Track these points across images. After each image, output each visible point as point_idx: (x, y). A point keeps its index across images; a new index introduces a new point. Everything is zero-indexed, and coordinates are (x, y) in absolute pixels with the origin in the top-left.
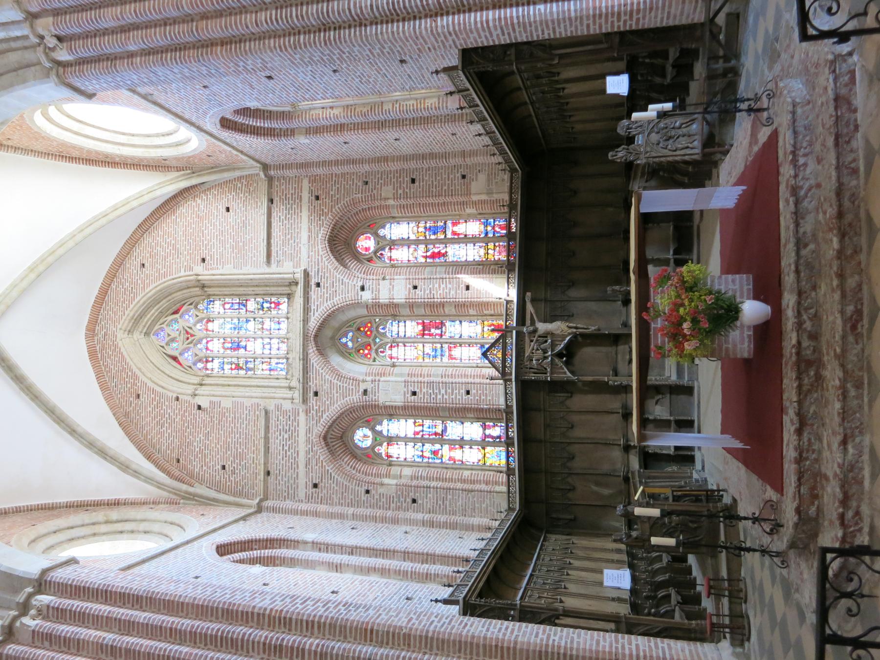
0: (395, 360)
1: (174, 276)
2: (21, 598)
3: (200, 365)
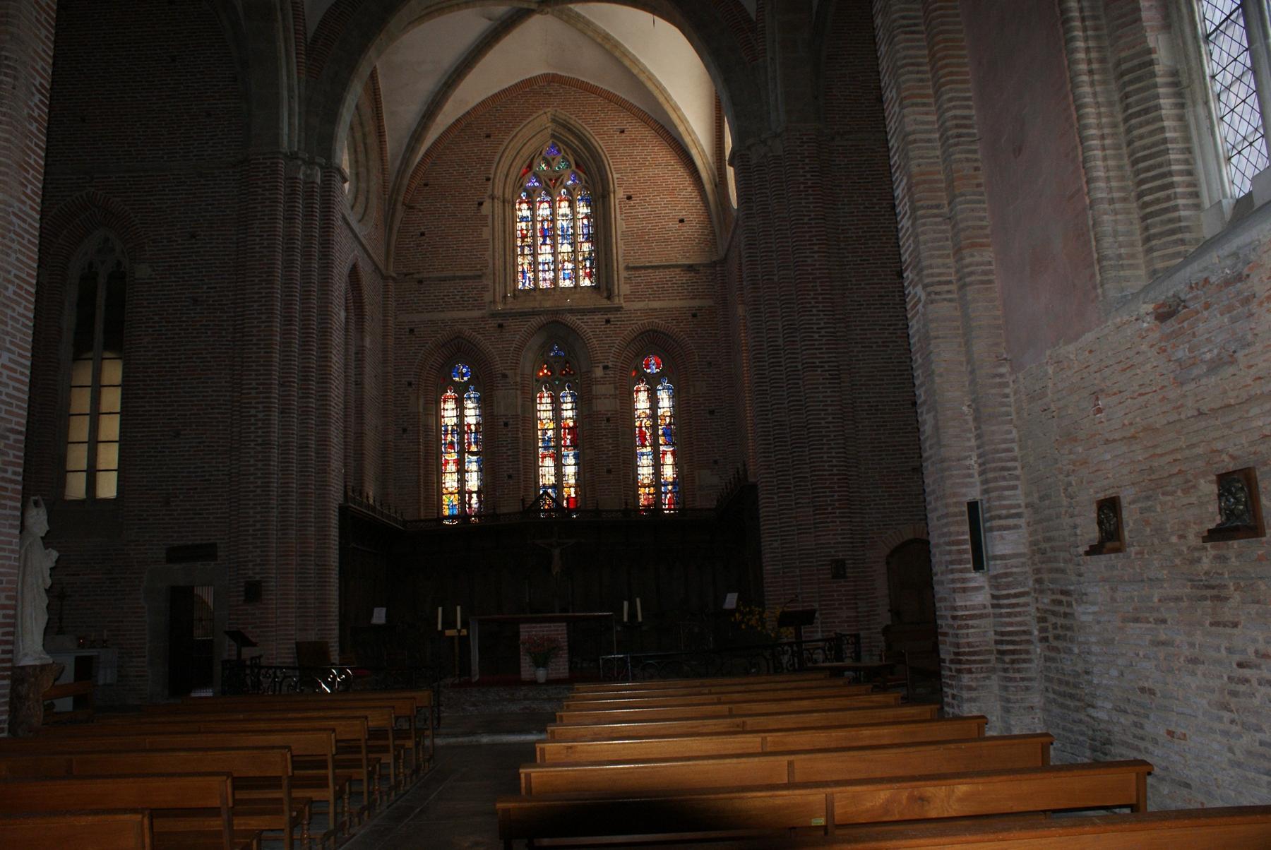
1: (612, 167)
2: (318, 160)
3: (523, 195)
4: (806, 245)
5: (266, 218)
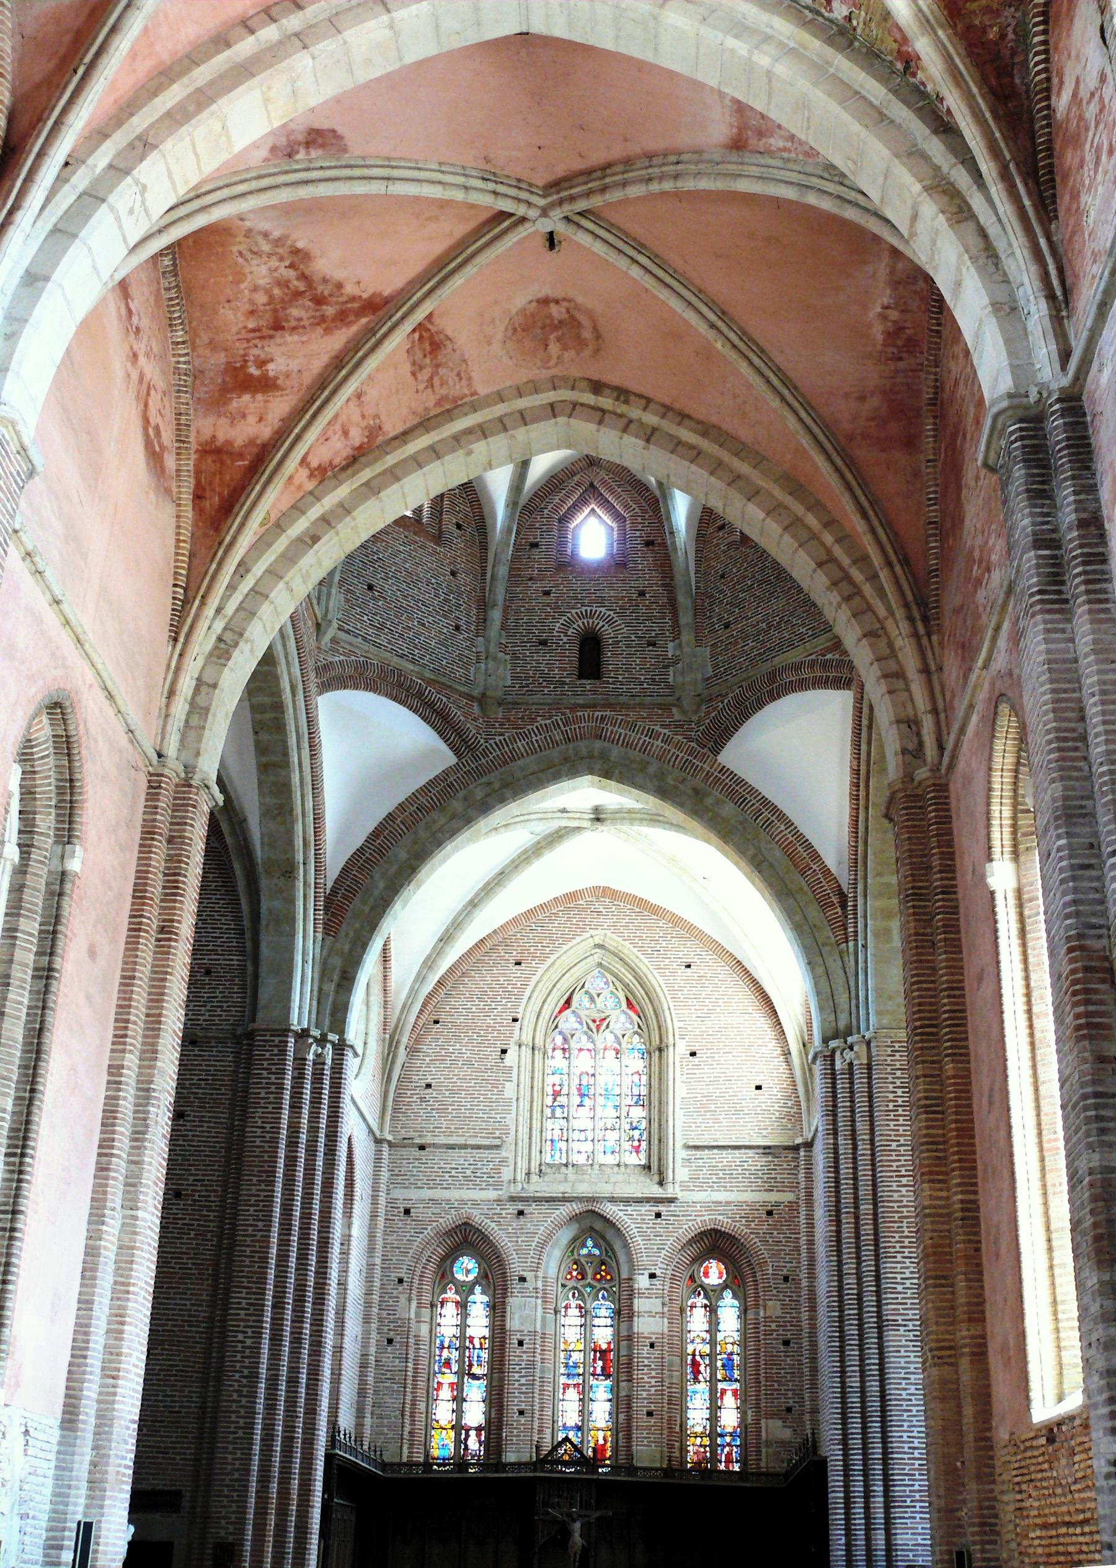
3: (559, 1040)
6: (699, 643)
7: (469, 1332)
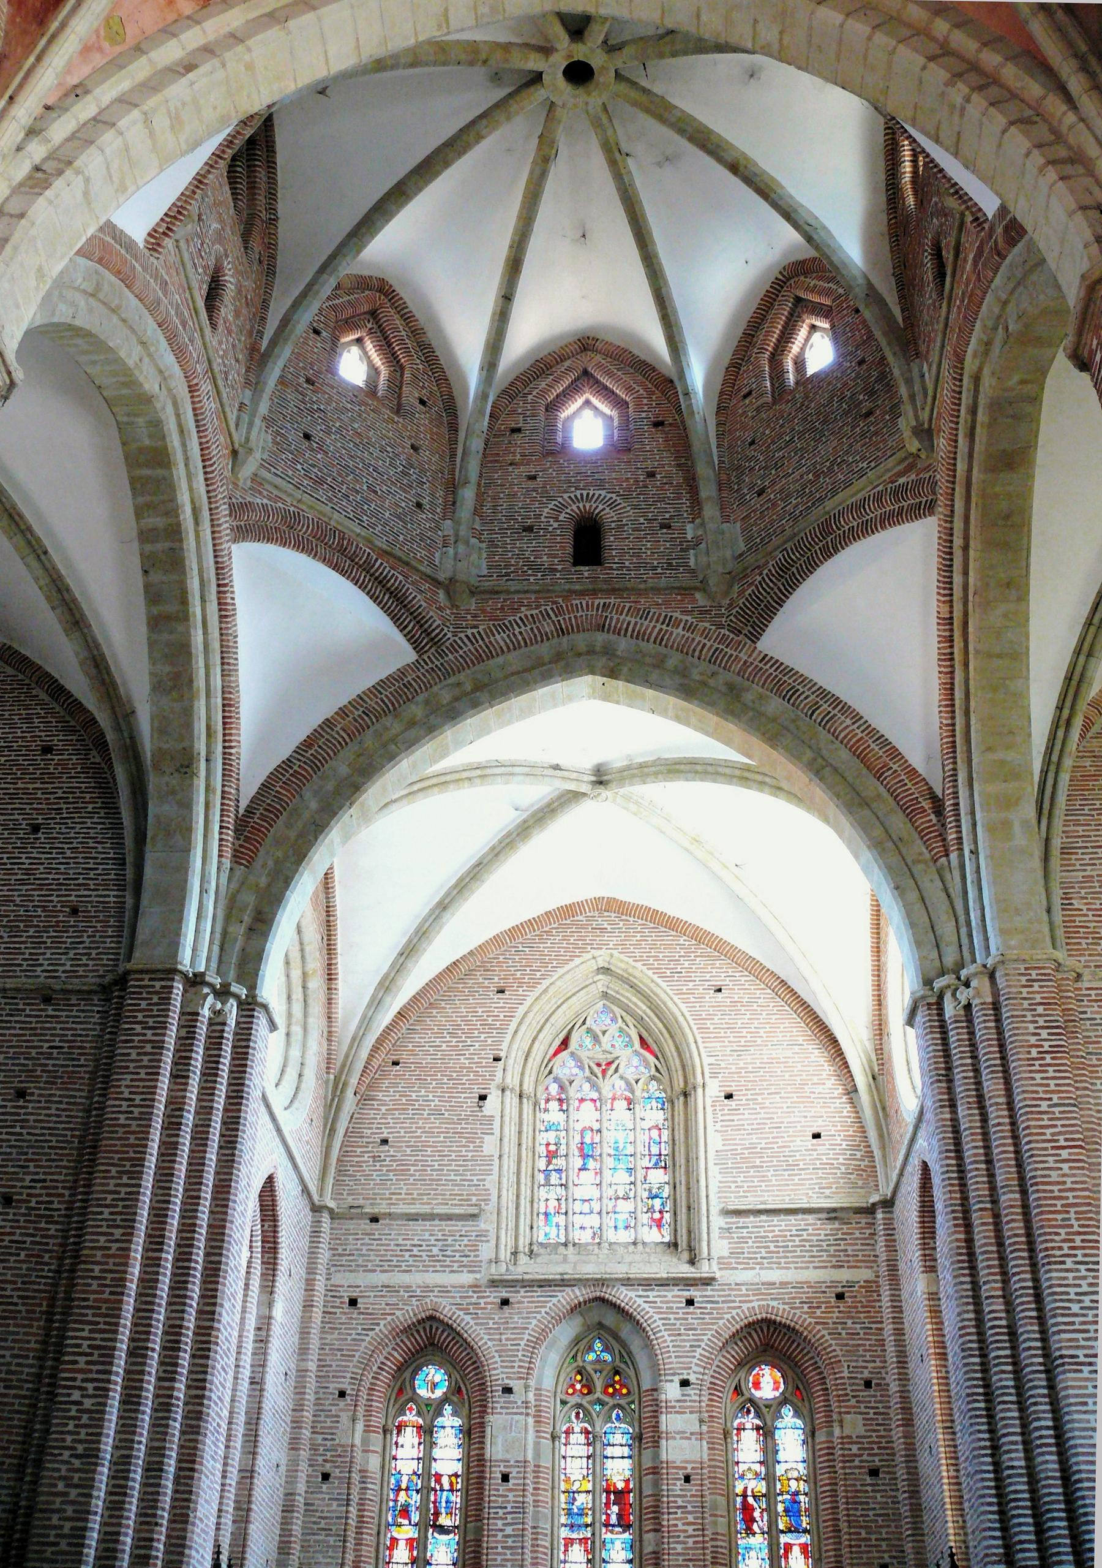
0: (563, 1440)
1: (701, 1045)
2: (235, 988)
3: (554, 1089)
4: (1046, 1149)
5: (143, 1071)
6: (726, 519)
7: (436, 1467)
